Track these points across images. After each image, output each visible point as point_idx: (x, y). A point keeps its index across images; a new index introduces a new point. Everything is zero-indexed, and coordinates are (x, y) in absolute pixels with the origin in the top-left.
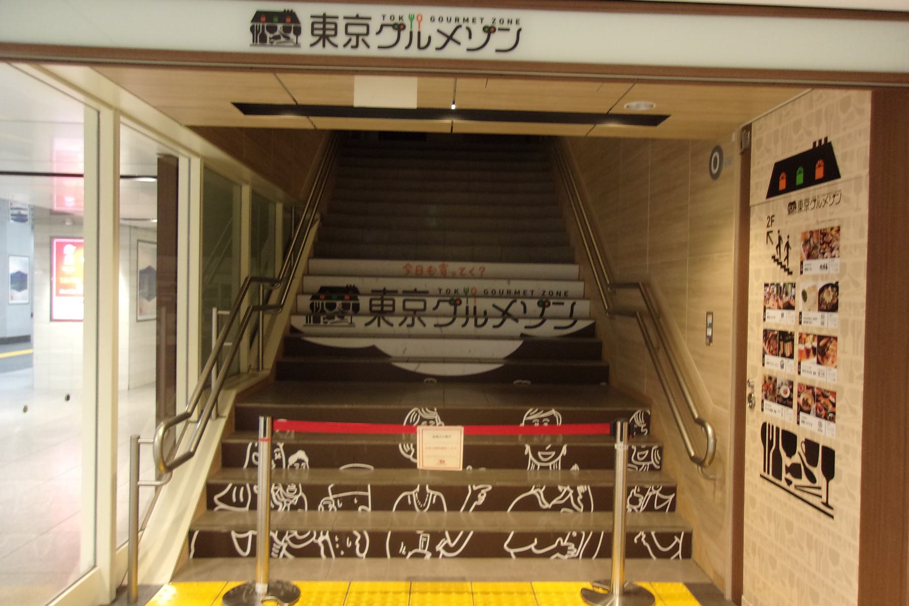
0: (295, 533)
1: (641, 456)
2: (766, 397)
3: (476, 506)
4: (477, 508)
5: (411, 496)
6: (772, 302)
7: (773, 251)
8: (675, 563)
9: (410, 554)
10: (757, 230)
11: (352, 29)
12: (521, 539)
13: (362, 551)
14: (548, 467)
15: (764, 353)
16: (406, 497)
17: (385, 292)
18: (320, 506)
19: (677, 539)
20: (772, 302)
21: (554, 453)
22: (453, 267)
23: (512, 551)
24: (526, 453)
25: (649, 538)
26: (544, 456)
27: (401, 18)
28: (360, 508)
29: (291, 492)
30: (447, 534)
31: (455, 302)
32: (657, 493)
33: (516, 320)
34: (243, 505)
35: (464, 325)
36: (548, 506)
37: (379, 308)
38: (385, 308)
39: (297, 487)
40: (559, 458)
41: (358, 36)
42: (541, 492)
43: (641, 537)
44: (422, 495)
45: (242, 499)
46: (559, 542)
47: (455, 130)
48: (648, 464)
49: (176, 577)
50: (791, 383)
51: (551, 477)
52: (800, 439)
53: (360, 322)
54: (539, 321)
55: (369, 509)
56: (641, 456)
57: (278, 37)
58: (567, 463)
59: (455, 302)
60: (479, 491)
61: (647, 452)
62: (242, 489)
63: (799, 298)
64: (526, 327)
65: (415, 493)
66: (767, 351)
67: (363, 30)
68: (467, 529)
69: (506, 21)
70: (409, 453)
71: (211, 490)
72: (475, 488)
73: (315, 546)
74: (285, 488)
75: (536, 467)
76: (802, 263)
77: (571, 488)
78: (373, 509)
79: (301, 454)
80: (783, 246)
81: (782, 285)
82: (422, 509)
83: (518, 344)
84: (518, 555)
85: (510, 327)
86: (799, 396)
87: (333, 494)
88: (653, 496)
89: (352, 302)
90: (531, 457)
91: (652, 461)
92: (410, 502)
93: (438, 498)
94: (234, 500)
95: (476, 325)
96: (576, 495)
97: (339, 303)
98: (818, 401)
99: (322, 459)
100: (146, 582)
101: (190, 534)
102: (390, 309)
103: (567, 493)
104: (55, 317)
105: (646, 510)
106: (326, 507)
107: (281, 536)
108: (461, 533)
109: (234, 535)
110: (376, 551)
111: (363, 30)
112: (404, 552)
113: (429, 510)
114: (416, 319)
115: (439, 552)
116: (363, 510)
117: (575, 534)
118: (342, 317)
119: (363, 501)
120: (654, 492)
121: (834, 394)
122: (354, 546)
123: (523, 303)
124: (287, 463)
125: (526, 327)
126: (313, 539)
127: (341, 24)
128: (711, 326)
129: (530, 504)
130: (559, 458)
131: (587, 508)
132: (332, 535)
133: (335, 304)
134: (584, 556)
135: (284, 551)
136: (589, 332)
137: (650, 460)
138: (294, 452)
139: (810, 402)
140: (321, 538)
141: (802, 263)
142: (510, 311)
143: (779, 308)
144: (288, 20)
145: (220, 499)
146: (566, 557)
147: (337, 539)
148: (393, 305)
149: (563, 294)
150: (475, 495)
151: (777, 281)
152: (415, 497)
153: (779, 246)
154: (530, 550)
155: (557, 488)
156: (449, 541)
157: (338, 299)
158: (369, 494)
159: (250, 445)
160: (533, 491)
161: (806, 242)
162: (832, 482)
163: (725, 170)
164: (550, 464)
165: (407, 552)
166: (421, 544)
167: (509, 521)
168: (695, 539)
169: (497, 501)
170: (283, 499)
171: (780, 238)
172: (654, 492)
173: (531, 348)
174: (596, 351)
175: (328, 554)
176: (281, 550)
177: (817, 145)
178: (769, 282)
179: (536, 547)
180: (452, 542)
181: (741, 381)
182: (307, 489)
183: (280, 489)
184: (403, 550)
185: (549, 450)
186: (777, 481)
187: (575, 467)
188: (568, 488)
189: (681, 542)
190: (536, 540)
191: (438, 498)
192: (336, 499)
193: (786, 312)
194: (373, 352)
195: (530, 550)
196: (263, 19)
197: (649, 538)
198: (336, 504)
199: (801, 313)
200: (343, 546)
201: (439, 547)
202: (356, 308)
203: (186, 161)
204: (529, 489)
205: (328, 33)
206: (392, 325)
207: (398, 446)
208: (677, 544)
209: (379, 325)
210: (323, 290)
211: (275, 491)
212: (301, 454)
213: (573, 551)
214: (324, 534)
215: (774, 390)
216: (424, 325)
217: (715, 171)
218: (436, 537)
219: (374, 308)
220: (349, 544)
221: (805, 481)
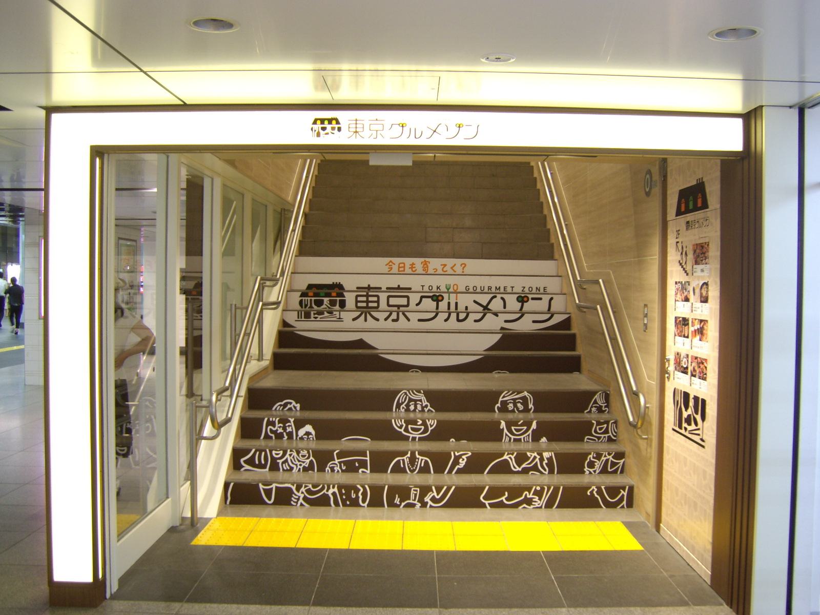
0: (310, 486)
1: (600, 429)
2: (676, 369)
3: (458, 468)
4: (460, 471)
5: (403, 460)
6: (679, 295)
7: (679, 258)
8: (622, 513)
9: (403, 504)
10: (671, 241)
12: (495, 492)
13: (364, 501)
14: (521, 439)
15: (675, 335)
16: (399, 460)
17: (369, 288)
18: (328, 468)
19: (622, 492)
20: (679, 295)
21: (525, 428)
22: (435, 263)
23: (487, 502)
24: (501, 428)
25: (600, 492)
26: (517, 430)
27: (438, 288)
28: (360, 470)
29: (303, 456)
30: (433, 488)
31: (437, 299)
32: (610, 458)
33: (496, 314)
34: (264, 467)
35: (446, 320)
36: (518, 469)
37: (364, 305)
38: (370, 305)
39: (308, 452)
40: (530, 432)
41: (399, 306)
42: (513, 457)
43: (593, 490)
44: (413, 460)
45: (263, 462)
46: (526, 494)
47: (437, 159)
48: (606, 435)
49: (220, 513)
50: (687, 356)
51: (522, 446)
52: (691, 397)
53: (347, 316)
54: (519, 315)
55: (368, 472)
56: (600, 429)
57: (327, 134)
58: (536, 437)
59: (437, 299)
60: (460, 456)
61: (605, 425)
62: (263, 453)
63: (692, 292)
64: (506, 321)
65: (406, 459)
66: (677, 334)
67: (403, 301)
68: (449, 483)
70: (401, 427)
71: (237, 454)
72: (457, 454)
73: (326, 497)
74: (298, 453)
75: (510, 440)
76: (693, 266)
77: (538, 454)
78: (371, 471)
79: (309, 428)
80: (684, 253)
81: (683, 283)
82: (412, 471)
83: (496, 338)
84: (491, 505)
85: (491, 322)
86: (691, 365)
87: (338, 459)
88: (607, 460)
89: (338, 299)
90: (505, 431)
91: (610, 434)
92: (402, 466)
93: (426, 462)
94: (257, 462)
95: (458, 320)
96: (542, 460)
97: (326, 300)
98: (700, 367)
99: (325, 431)
100: (201, 517)
101: (226, 485)
102: (375, 305)
103: (535, 458)
105: (600, 473)
106: (332, 469)
107: (298, 489)
108: (445, 488)
109: (261, 486)
110: (376, 502)
111: (403, 301)
112: (398, 503)
113: (418, 473)
114: (401, 313)
115: (427, 503)
116: (363, 472)
117: (538, 488)
118: (330, 313)
119: (363, 464)
120: (608, 457)
121: (706, 360)
122: (357, 497)
123: (502, 298)
124: (297, 435)
125: (506, 321)
126: (325, 491)
128: (646, 316)
129: (504, 468)
130: (530, 432)
131: (551, 471)
132: (340, 488)
133: (323, 301)
134: (546, 507)
135: (301, 501)
136: (566, 324)
137: (608, 433)
138: (303, 426)
139: (696, 368)
140: (331, 491)
141: (693, 266)
142: (489, 307)
143: (682, 301)
144: (334, 122)
145: (245, 462)
146: (532, 506)
147: (344, 492)
148: (378, 302)
149: (542, 291)
150: (457, 459)
151: (681, 280)
152: (407, 461)
153: (682, 254)
154: (502, 500)
155: (526, 454)
156: (435, 494)
157: (326, 296)
158: (368, 459)
159: (266, 419)
160: (506, 457)
161: (695, 251)
162: (705, 423)
163: (653, 191)
164: (522, 437)
165: (401, 502)
166: (412, 496)
167: (486, 480)
168: (635, 490)
169: (476, 465)
170: (297, 462)
171: (682, 248)
172: (608, 457)
173: (509, 340)
174: (570, 342)
175: (337, 504)
176: (298, 499)
177: (698, 182)
178: (678, 280)
179: (507, 499)
180: (438, 495)
181: (663, 359)
182: (316, 454)
183: (295, 454)
184: (397, 501)
185: (521, 425)
186: (680, 431)
187: (544, 439)
188: (535, 454)
189: (625, 494)
190: (506, 493)
191: (426, 462)
192: (340, 463)
193: (685, 303)
194: (361, 344)
195: (502, 500)
196: (319, 122)
197: (600, 492)
198: (341, 467)
199: (692, 303)
200: (349, 497)
201: (427, 499)
202: (343, 304)
203: (210, 180)
204: (502, 455)
206: (377, 320)
207: (391, 421)
208: (623, 495)
209: (366, 320)
210: (310, 287)
211: (290, 455)
212: (309, 428)
213: (537, 502)
214: (333, 487)
215: (680, 363)
216: (409, 320)
217: (647, 190)
218: (425, 490)
219: (360, 305)
220: (354, 496)
221: (693, 427)
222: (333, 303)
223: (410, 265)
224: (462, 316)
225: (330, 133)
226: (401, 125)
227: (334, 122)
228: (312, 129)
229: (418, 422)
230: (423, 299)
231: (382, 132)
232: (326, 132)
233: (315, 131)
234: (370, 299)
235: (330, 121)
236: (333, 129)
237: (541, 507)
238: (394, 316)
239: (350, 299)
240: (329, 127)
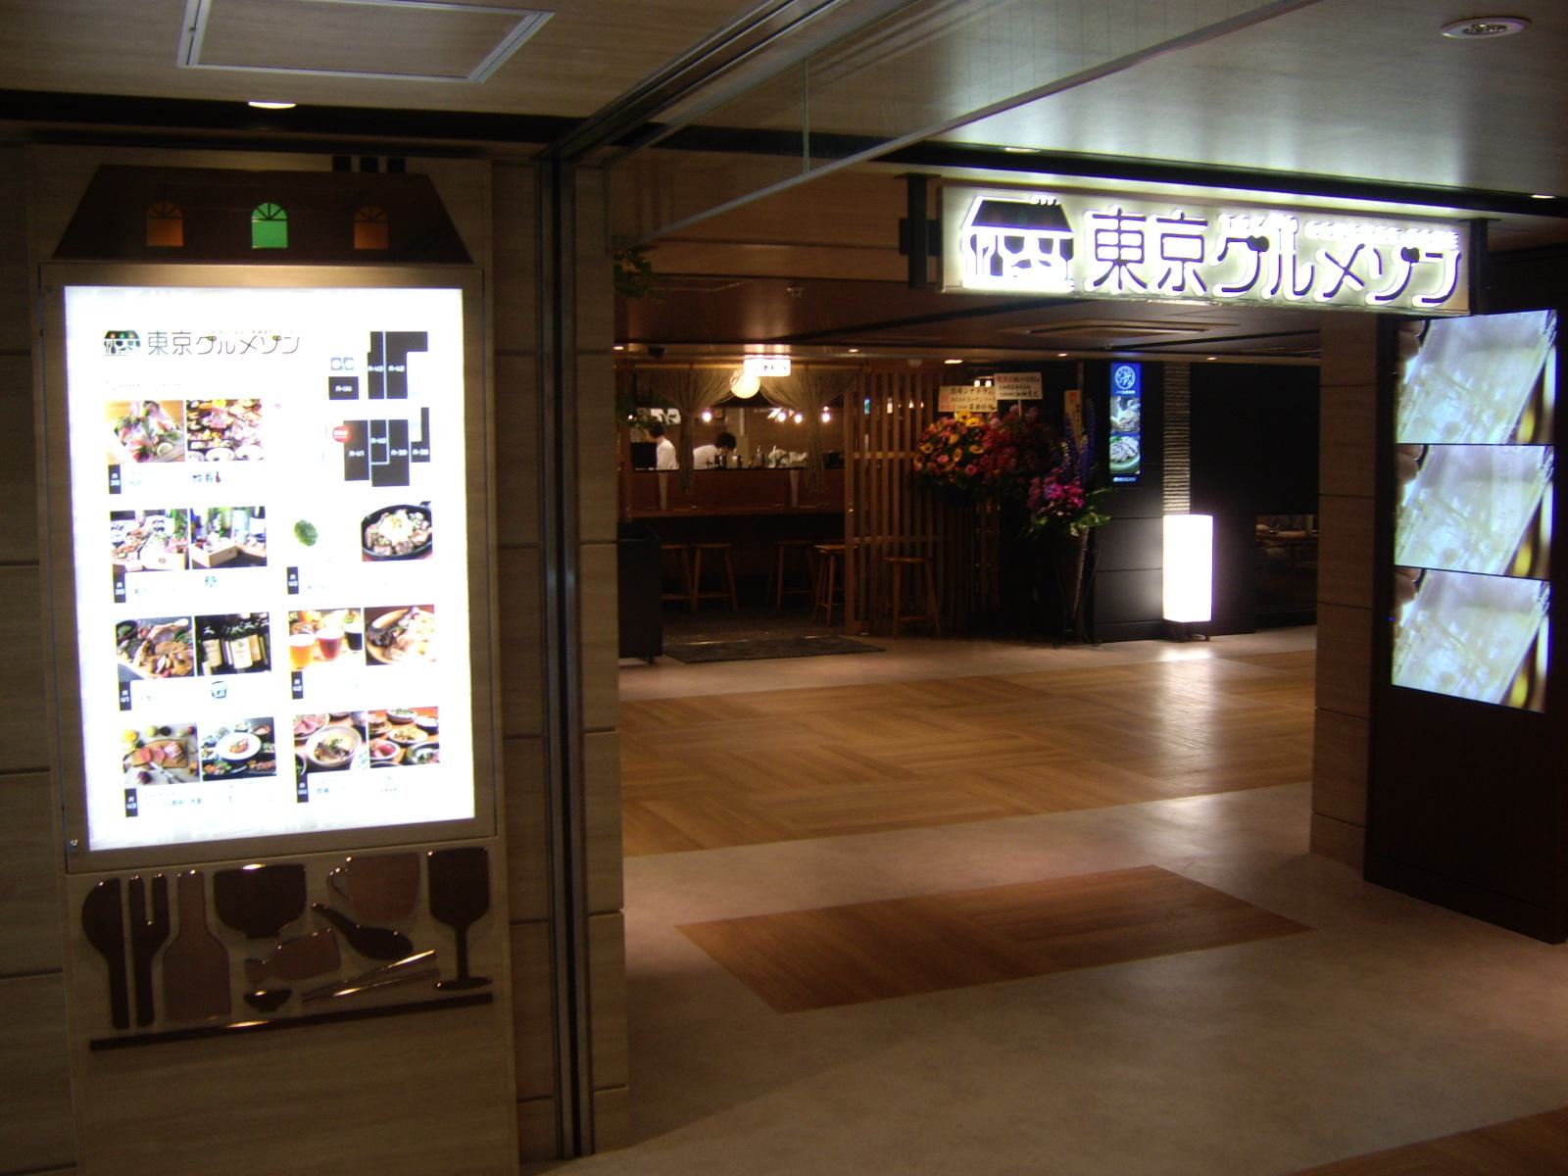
11: (177, 341)
41: (183, 346)
57: (123, 349)
67: (186, 341)
69: (1056, 247)
104: (1166, 240)
111: (186, 341)
127: (170, 337)
144: (131, 336)
190: (804, 455)
196: (113, 336)
205: (160, 345)
223: (201, 547)
224: (230, 350)
227: (131, 336)
228: (105, 343)
231: (1197, 266)
234: (1126, 239)
236: (130, 343)
237: (246, 731)
238: (180, 351)
239: (143, 339)
240: (125, 342)
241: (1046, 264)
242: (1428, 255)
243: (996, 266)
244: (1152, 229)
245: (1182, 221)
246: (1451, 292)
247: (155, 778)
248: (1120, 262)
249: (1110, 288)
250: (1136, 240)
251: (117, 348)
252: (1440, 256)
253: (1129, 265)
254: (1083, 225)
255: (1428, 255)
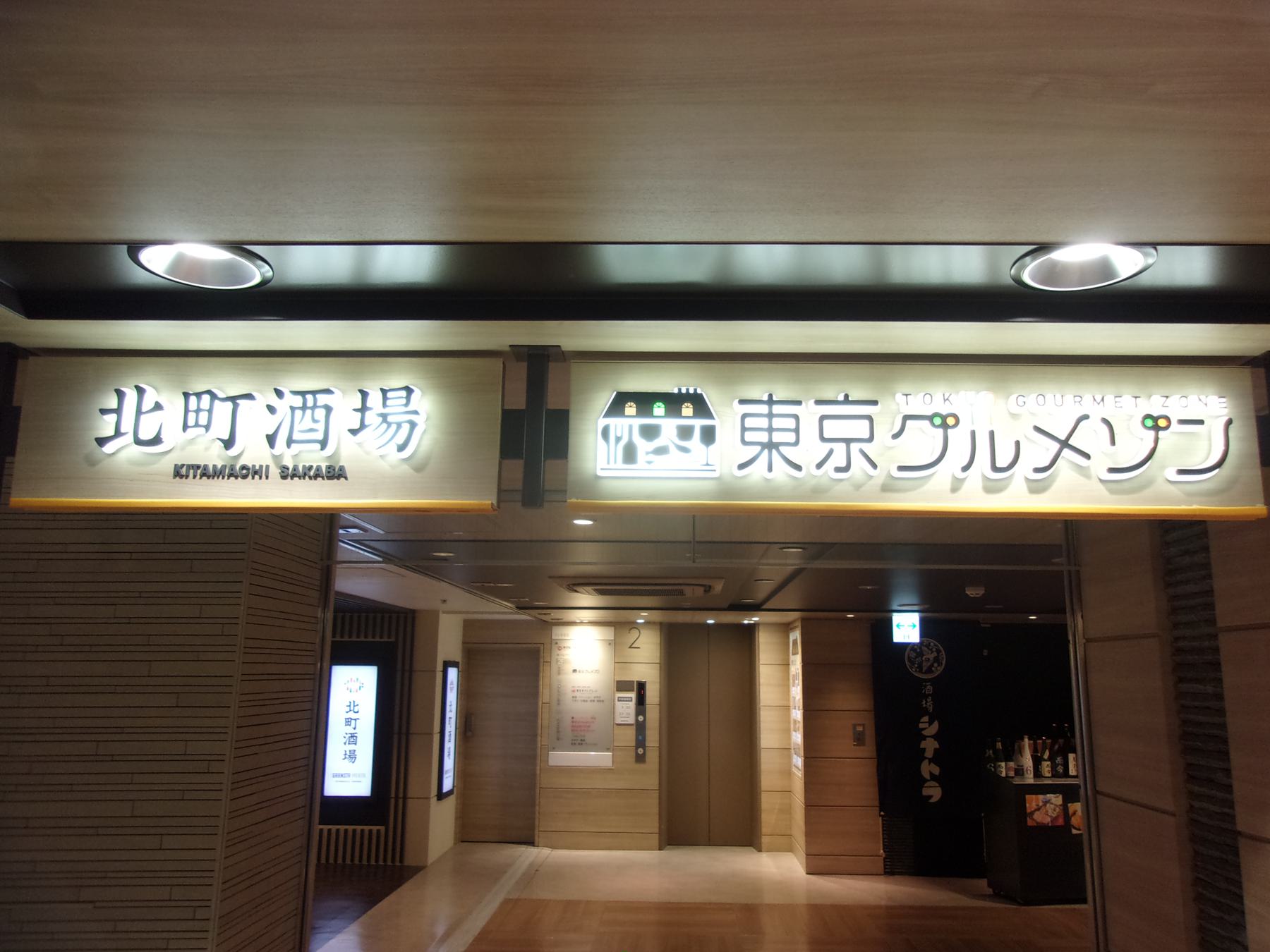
41: (848, 441)
57: (661, 451)
67: (861, 429)
69: (697, 433)
104: (826, 422)
111: (861, 429)
222: (685, 433)
225: (672, 449)
226: (938, 421)
227: (687, 410)
229: (931, 797)
230: (909, 422)
231: (866, 447)
232: (657, 443)
233: (618, 439)
234: (777, 423)
235: (673, 402)
236: (685, 433)
238: (839, 459)
241: (685, 450)
242: (1182, 422)
243: (630, 454)
244: (809, 413)
245: (847, 401)
246: (1219, 464)
247: (335, 787)
248: (771, 446)
249: (757, 472)
250: (791, 423)
251: (643, 446)
252: (1201, 422)
253: (781, 448)
254: (726, 416)
255: (1182, 422)
